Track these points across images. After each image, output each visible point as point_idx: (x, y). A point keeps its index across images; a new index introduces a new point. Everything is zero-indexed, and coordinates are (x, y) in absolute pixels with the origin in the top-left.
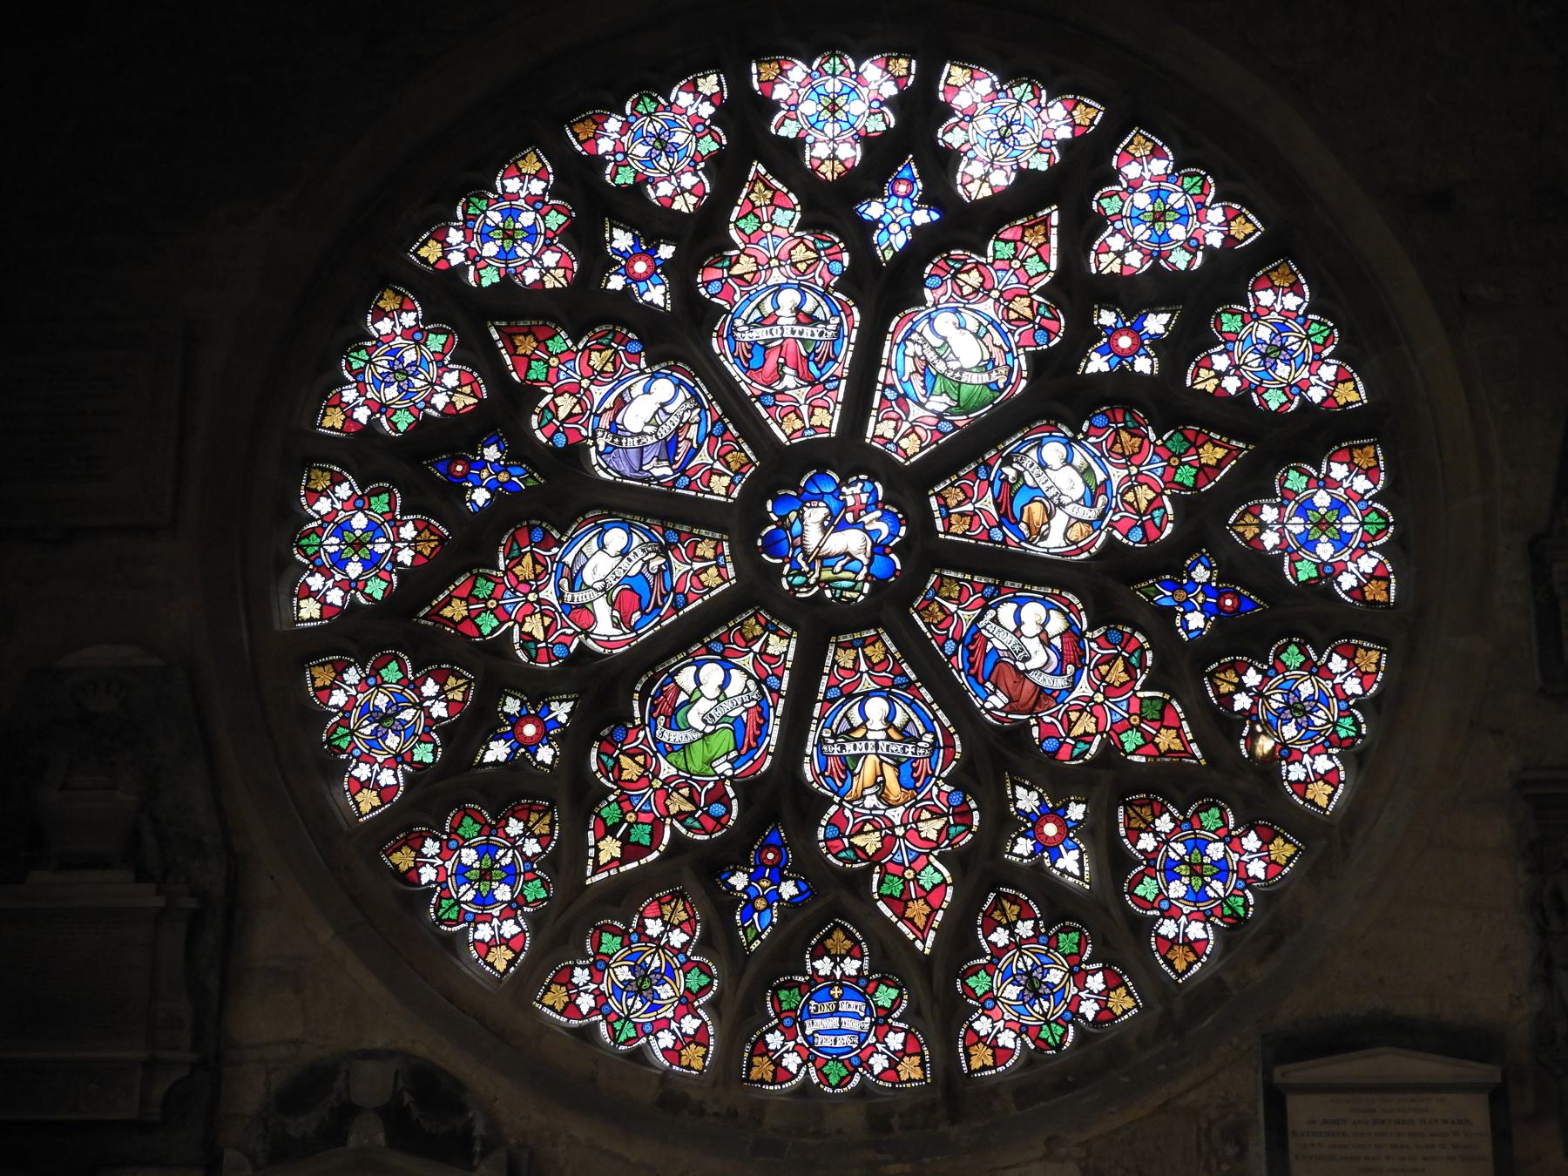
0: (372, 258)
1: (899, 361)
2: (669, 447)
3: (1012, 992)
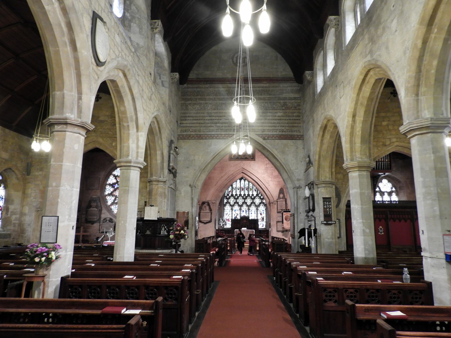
0: (110, 174)
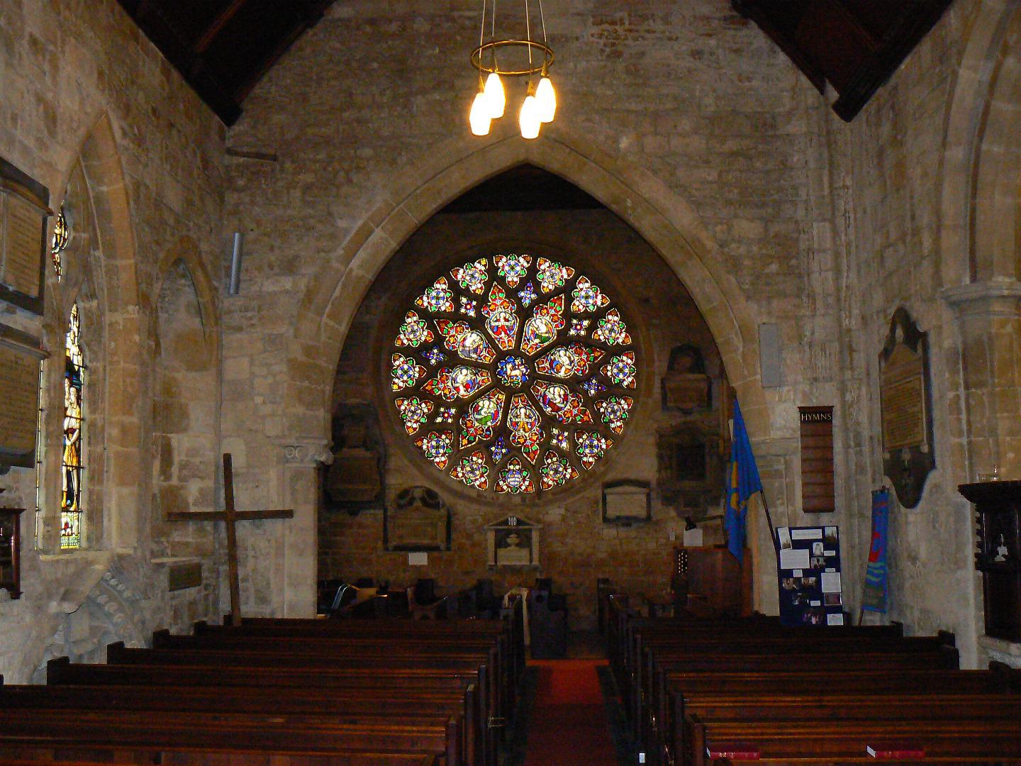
1: (528, 330)
2: (475, 350)
3: (552, 472)
